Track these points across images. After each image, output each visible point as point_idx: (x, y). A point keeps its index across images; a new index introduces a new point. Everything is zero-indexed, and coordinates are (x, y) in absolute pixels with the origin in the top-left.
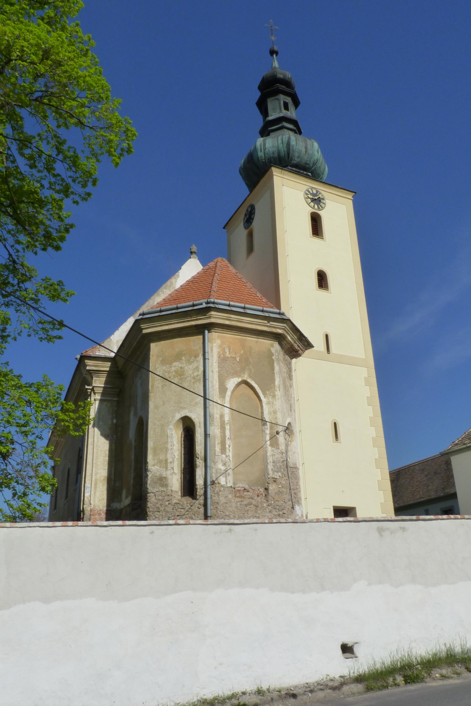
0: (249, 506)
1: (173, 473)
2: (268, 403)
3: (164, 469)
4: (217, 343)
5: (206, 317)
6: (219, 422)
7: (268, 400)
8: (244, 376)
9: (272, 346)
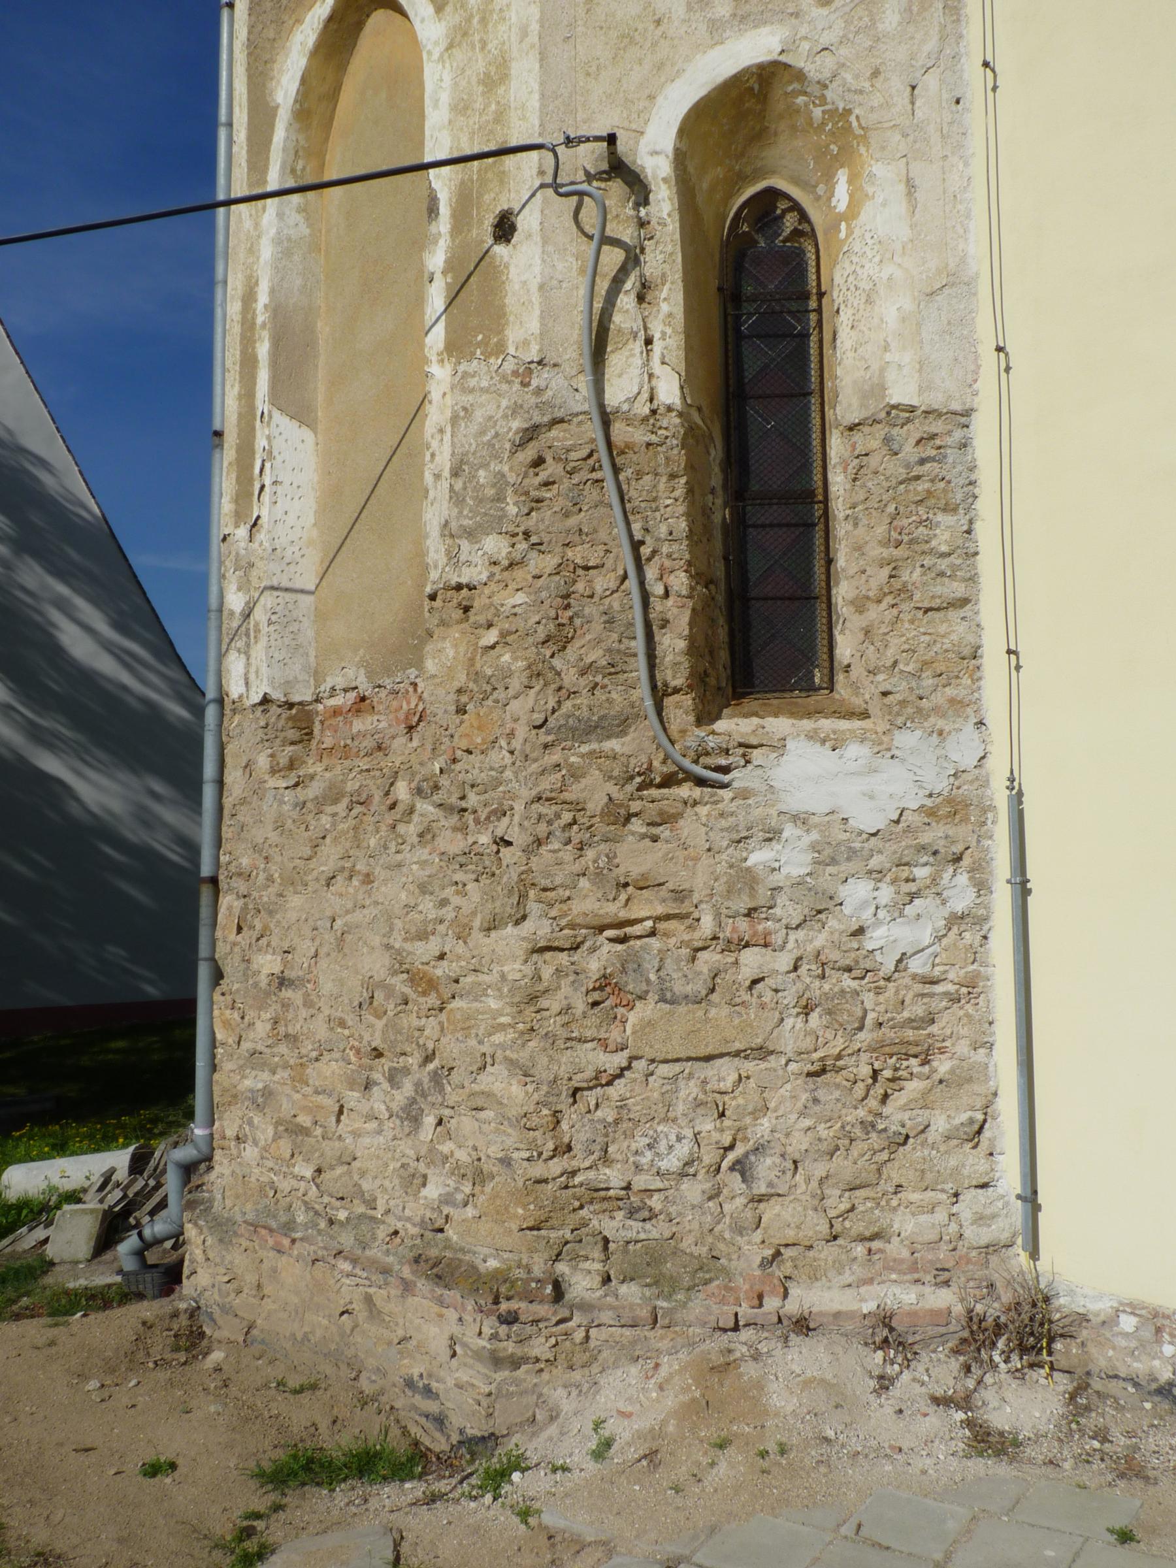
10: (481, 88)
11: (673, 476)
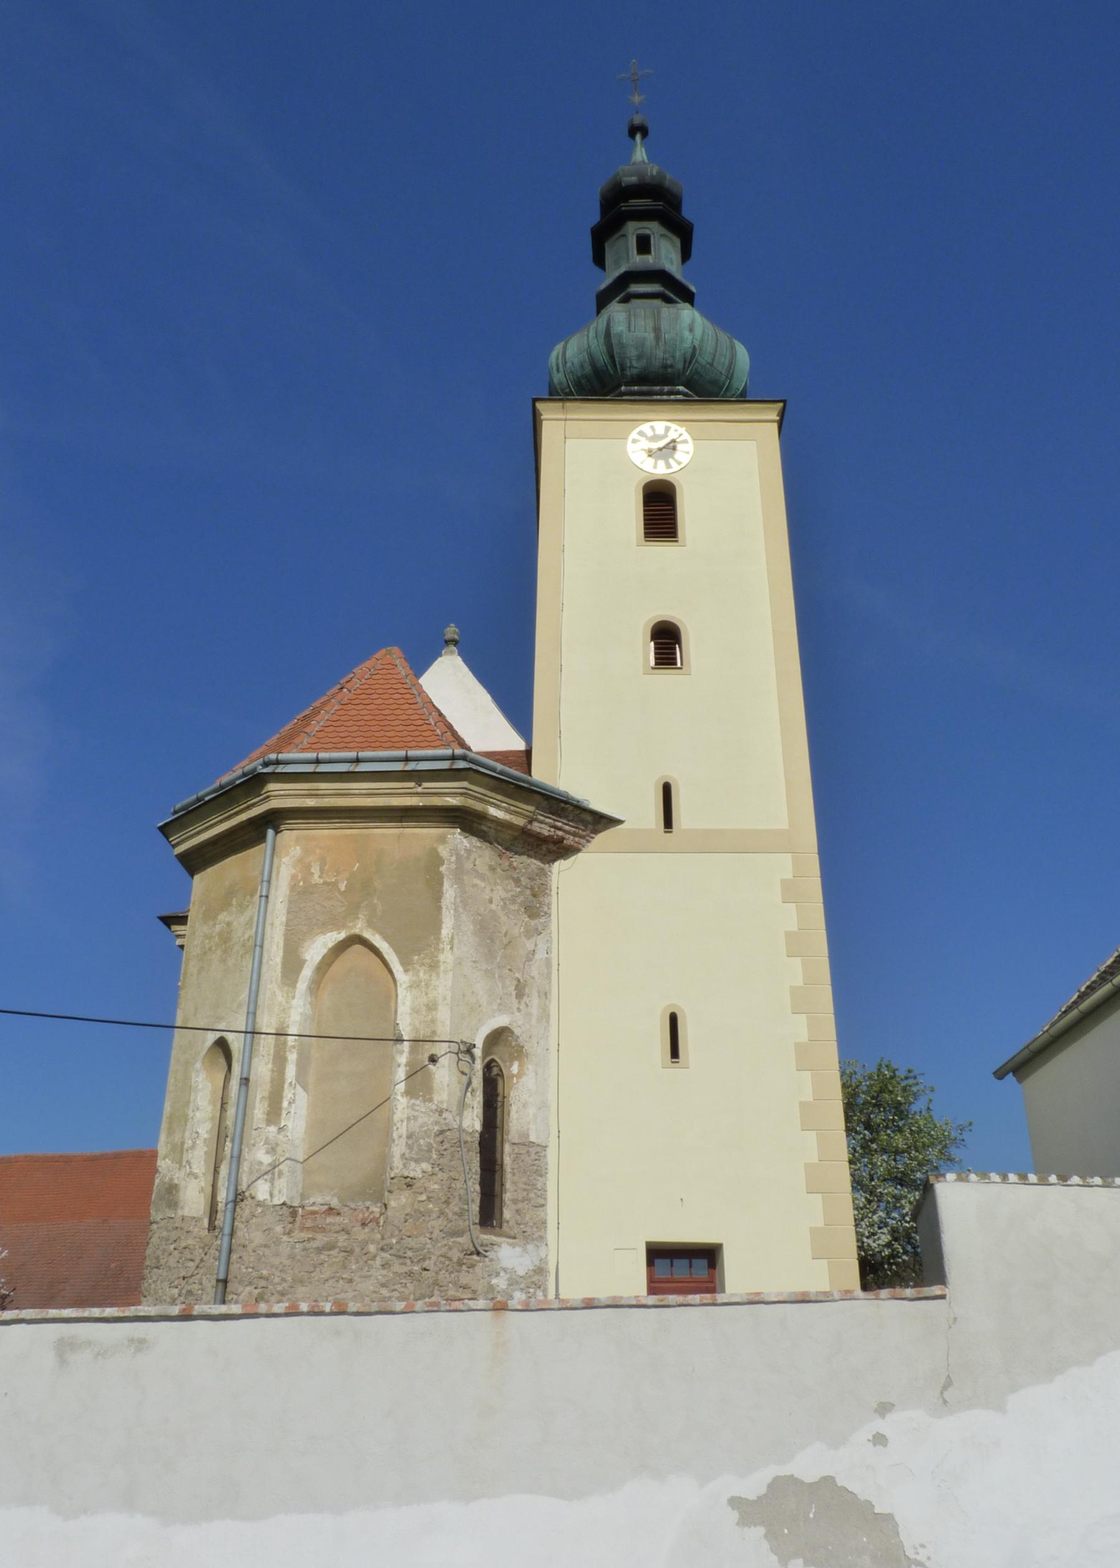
0: (327, 1253)
1: (189, 1174)
2: (413, 986)
3: (178, 1165)
4: (292, 854)
5: (261, 797)
6: (273, 1045)
7: (415, 978)
8: (355, 926)
9: (442, 840)
10: (425, 1008)
11: (477, 1153)
